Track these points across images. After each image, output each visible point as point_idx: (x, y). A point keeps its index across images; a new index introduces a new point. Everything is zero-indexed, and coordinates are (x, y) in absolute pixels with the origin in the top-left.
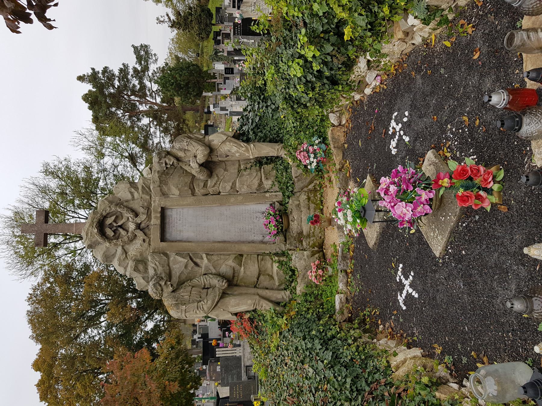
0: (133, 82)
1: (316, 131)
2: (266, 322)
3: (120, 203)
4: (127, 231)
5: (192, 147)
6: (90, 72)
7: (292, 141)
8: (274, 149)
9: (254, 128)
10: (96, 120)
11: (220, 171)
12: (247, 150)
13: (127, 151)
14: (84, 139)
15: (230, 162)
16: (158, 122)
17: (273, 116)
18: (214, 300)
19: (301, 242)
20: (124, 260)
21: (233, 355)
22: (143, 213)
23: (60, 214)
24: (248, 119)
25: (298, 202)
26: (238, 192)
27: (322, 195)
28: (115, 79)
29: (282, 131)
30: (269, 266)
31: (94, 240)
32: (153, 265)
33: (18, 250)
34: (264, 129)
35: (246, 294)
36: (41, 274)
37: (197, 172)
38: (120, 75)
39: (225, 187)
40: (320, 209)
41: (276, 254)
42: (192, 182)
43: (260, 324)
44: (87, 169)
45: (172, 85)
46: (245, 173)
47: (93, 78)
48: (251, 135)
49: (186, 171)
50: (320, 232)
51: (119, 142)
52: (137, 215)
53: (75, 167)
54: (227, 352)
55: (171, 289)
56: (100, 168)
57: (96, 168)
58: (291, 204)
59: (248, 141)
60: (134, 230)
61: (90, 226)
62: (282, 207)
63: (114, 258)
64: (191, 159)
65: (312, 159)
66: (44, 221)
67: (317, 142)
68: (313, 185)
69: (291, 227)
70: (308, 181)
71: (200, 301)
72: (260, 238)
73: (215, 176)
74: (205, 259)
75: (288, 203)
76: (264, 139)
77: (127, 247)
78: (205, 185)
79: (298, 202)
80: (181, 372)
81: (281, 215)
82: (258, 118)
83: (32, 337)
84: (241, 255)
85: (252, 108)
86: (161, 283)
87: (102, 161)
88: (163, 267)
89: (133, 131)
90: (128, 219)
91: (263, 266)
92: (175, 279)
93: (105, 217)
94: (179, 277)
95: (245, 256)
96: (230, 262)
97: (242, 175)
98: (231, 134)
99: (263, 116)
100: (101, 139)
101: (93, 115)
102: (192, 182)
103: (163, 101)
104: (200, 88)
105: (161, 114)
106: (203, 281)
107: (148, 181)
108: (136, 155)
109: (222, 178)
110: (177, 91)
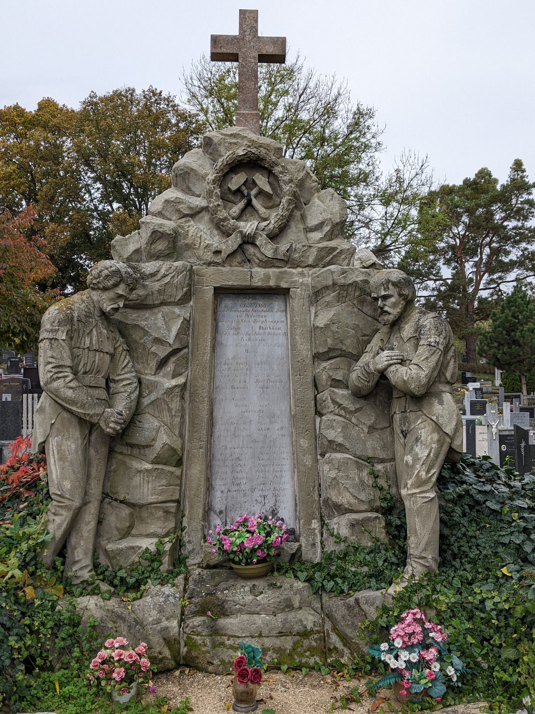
0: (514, 250)
1: (477, 664)
2: (23, 523)
3: (298, 203)
4: (239, 218)
5: (427, 354)
6: (531, 180)
7: (446, 598)
8: (425, 550)
9: (471, 496)
10: (447, 191)
11: (369, 417)
12: (420, 483)
13: (395, 242)
14: (413, 172)
15: (389, 439)
16: (445, 291)
17: (504, 544)
18: (73, 402)
19: (202, 611)
20: (178, 211)
21: (25, 425)
22: (276, 250)
23: (289, 138)
24: (491, 481)
25: (296, 605)
26: (323, 455)
27: (313, 668)
28: (519, 220)
29: (468, 567)
30: (152, 529)
31: (222, 149)
32: (163, 271)
33: (232, 75)
34: (470, 522)
35: (88, 476)
36: (191, 109)
37: (368, 365)
38: (527, 229)
39: (332, 427)
40: (279, 663)
41: (179, 544)
42: (343, 354)
43: (21, 506)
44: (364, 178)
45: (513, 316)
46: (365, 473)
47: (519, 185)
48: (453, 490)
49: (369, 342)
50: (223, 661)
51: (409, 228)
52: (274, 237)
53: (366, 159)
54: (30, 414)
55: (108, 307)
56: (365, 200)
57: (365, 192)
58: (294, 586)
59: (441, 482)
60: (241, 232)
61: (251, 141)
62: (287, 559)
63: (183, 191)
64: (396, 352)
65: (404, 655)
66: (264, 52)
67: (450, 671)
68: (339, 645)
69: (242, 583)
70: (348, 631)
71: (75, 373)
72: (218, 504)
73: (358, 406)
74: (174, 382)
75: (296, 577)
76: (446, 522)
77: (206, 217)
78: (336, 383)
79: (296, 605)
80: (8, 332)
81: (269, 561)
82: (496, 507)
83: (93, 95)
84: (179, 463)
85: (516, 492)
87: (376, 201)
88: (159, 291)
89: (430, 252)
90: (265, 220)
91: (152, 514)
92: (133, 317)
93: (269, 172)
94: (137, 326)
95: (177, 471)
96: (165, 437)
97: (360, 468)
99: (501, 520)
100: (414, 198)
101: (454, 186)
102: (343, 354)
103: (482, 301)
104: (510, 364)
105: (459, 298)
106: (126, 377)
107: (347, 261)
108: (387, 258)
109: (354, 420)
110: (502, 325)
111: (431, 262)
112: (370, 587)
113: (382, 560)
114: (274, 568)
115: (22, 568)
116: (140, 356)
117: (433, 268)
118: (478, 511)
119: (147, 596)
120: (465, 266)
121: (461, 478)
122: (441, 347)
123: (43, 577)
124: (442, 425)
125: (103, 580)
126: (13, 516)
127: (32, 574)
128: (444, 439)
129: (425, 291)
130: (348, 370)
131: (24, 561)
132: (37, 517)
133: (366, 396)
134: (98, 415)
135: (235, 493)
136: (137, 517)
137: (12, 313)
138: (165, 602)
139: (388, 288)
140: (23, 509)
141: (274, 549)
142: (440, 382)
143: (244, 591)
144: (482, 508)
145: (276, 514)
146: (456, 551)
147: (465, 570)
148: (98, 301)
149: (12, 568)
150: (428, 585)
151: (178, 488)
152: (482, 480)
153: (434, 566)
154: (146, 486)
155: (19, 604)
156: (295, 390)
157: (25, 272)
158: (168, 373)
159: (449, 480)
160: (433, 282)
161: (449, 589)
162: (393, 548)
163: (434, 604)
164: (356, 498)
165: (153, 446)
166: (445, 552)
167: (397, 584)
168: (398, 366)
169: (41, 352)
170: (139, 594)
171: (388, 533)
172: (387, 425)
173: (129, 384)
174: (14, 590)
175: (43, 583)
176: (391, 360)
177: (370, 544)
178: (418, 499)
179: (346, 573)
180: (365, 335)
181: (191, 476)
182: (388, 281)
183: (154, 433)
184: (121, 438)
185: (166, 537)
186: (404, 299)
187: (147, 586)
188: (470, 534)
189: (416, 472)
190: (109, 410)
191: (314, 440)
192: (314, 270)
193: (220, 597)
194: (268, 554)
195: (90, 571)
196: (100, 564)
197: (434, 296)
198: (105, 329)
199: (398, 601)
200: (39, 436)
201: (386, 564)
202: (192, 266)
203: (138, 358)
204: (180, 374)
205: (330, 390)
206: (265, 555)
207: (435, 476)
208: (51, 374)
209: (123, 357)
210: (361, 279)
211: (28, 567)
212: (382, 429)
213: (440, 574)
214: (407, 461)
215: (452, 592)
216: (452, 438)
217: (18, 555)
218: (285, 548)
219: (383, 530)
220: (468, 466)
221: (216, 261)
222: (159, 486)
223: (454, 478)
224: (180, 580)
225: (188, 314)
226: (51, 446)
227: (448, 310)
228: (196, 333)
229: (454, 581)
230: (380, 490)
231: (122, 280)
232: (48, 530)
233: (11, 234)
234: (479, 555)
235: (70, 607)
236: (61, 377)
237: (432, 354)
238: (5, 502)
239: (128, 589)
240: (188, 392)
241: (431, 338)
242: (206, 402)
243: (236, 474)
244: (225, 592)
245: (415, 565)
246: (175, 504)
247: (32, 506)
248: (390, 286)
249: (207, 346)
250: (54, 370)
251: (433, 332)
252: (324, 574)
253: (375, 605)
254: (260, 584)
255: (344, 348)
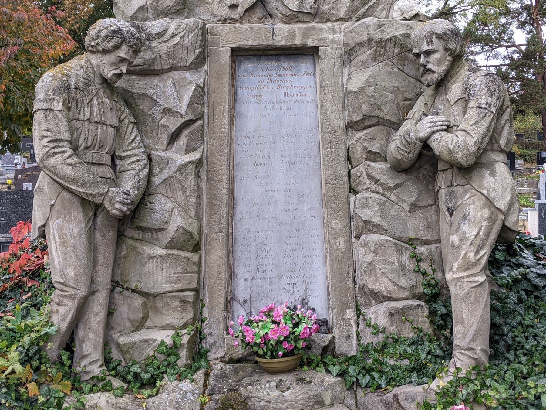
5: (476, 118)
8: (473, 340)
9: (529, 280)
11: (411, 193)
12: (468, 266)
15: (434, 218)
16: (518, 60)
18: (74, 181)
25: (328, 401)
26: (358, 237)
29: (523, 359)
32: (171, 31)
34: (527, 309)
35: (95, 263)
37: (408, 133)
39: (368, 206)
42: (381, 122)
43: (25, 297)
46: (406, 257)
48: (507, 274)
49: (411, 107)
55: (109, 73)
59: (494, 264)
62: (319, 352)
64: (441, 117)
69: (267, 377)
71: (75, 148)
72: (242, 293)
73: (398, 181)
74: (187, 158)
75: (327, 371)
76: (498, 310)
78: (373, 156)
79: (328, 401)
84: (197, 248)
86: (124, 48)
88: (168, 54)
89: (500, 14)
91: (167, 304)
92: (139, 85)
94: (144, 95)
95: (195, 257)
96: (179, 219)
97: (399, 251)
98: (510, 222)
102: (381, 122)
107: (385, 13)
109: (393, 197)
111: (502, 26)
112: (411, 382)
113: (425, 352)
114: (303, 362)
115: (23, 363)
116: (149, 129)
117: (504, 33)
118: (536, 297)
119: (163, 392)
120: (541, 30)
121: (518, 260)
122: (493, 109)
123: (47, 373)
124: (494, 199)
125: (115, 376)
126: (15, 308)
127: (37, 370)
128: (497, 216)
129: (495, 60)
130: (387, 140)
131: (27, 354)
132: (41, 308)
133: (407, 169)
134: (101, 194)
135: (260, 281)
136: (151, 307)
137: (29, 95)
138: (183, 398)
139: (432, 42)
140: (26, 300)
141: (302, 341)
142: (493, 151)
143: (270, 387)
144: (541, 294)
145: (306, 304)
146: (510, 342)
147: (520, 363)
148: (98, 67)
149: (13, 362)
150: (476, 379)
151: (196, 275)
152: (542, 262)
153: (483, 358)
154: (160, 274)
155: (22, 401)
156: (325, 165)
157: (41, 48)
158: (181, 148)
159: (503, 263)
160: (504, 49)
161: (500, 384)
162: (438, 339)
163: (483, 400)
164: (396, 284)
165: (166, 229)
166: (498, 343)
167: (441, 378)
168: (443, 133)
169: (35, 124)
170: (154, 391)
171: (432, 323)
172: (432, 203)
173: (138, 161)
174: (14, 387)
175: (48, 379)
176: (435, 126)
177: (411, 335)
178: (465, 284)
179: (384, 367)
180: (406, 100)
181: (210, 263)
182: (432, 33)
183: (167, 215)
184: (131, 221)
185: (184, 329)
186: (450, 55)
187: (163, 382)
188: (527, 322)
189: (463, 253)
190: (113, 189)
191: (347, 221)
192: (346, 24)
193: (243, 393)
194: (296, 347)
195: (101, 366)
196: (112, 359)
197: (505, 65)
198: (108, 98)
199: (442, 397)
200: (38, 219)
201: (430, 357)
202: (204, 24)
203: (147, 131)
204: (195, 149)
205: (366, 164)
206: (292, 347)
207: (485, 258)
208: (47, 149)
209: (129, 130)
210: (402, 33)
211: (32, 362)
212: (426, 207)
213: (490, 368)
214: (452, 242)
215: (504, 386)
216: (506, 215)
217: (21, 349)
218: (317, 340)
219: (427, 320)
220: (527, 247)
221: (232, 16)
222: (175, 274)
223: (510, 261)
224: (200, 375)
225: (202, 80)
226: (51, 230)
227: (522, 81)
228: (211, 103)
229: (507, 375)
230: (423, 275)
231: (123, 41)
232: (52, 322)
233: (25, 5)
234: (537, 346)
235: (78, 404)
236: (58, 153)
237: (483, 118)
238: (7, 293)
239: (143, 386)
240: (204, 169)
241: (481, 98)
242: (225, 180)
243: (261, 260)
244: (248, 388)
245: (461, 357)
246: (192, 293)
247: (36, 296)
248: (434, 39)
249: (225, 117)
250: (50, 145)
251: (484, 92)
252: (358, 368)
253: (416, 401)
254: (288, 378)
255: (382, 115)
